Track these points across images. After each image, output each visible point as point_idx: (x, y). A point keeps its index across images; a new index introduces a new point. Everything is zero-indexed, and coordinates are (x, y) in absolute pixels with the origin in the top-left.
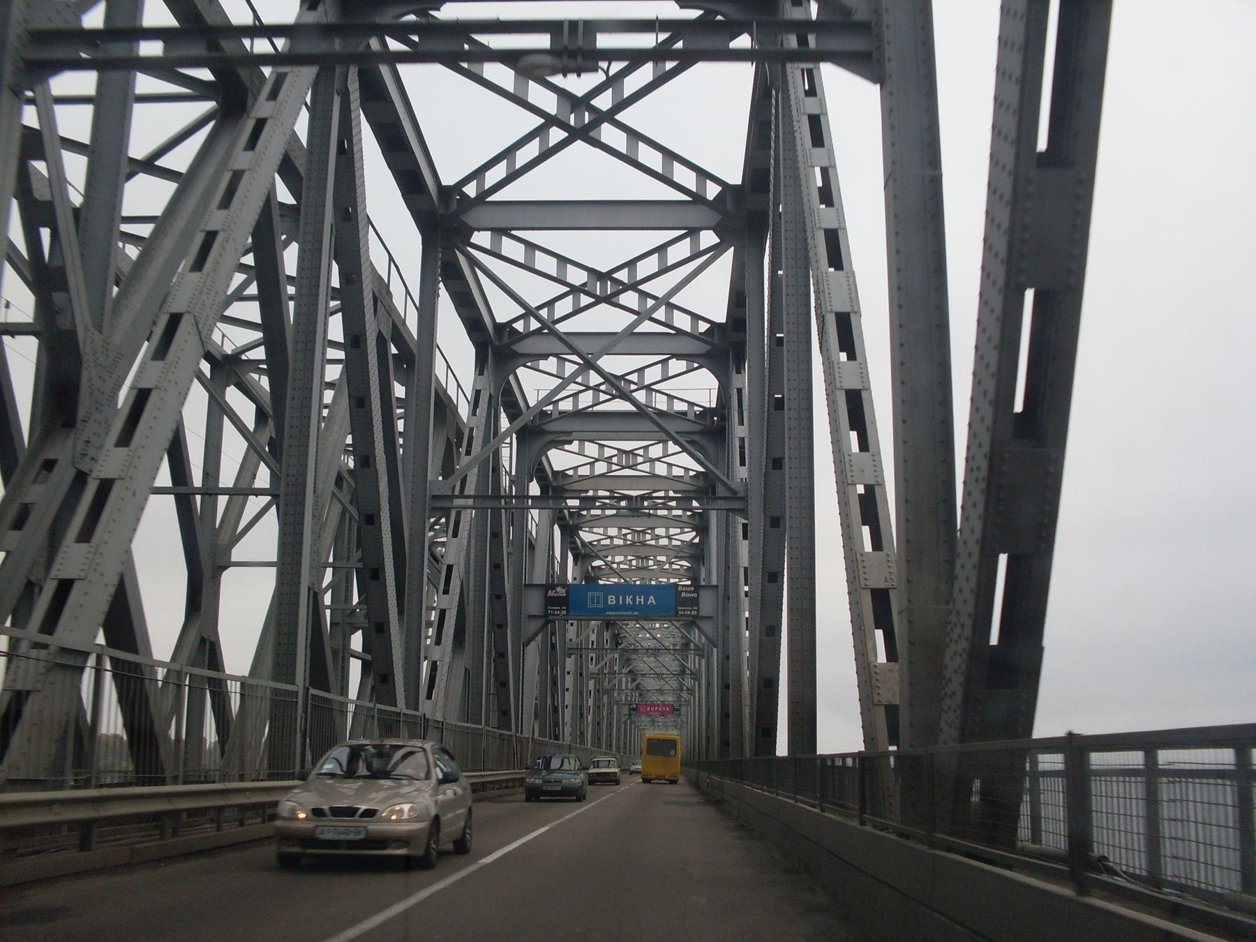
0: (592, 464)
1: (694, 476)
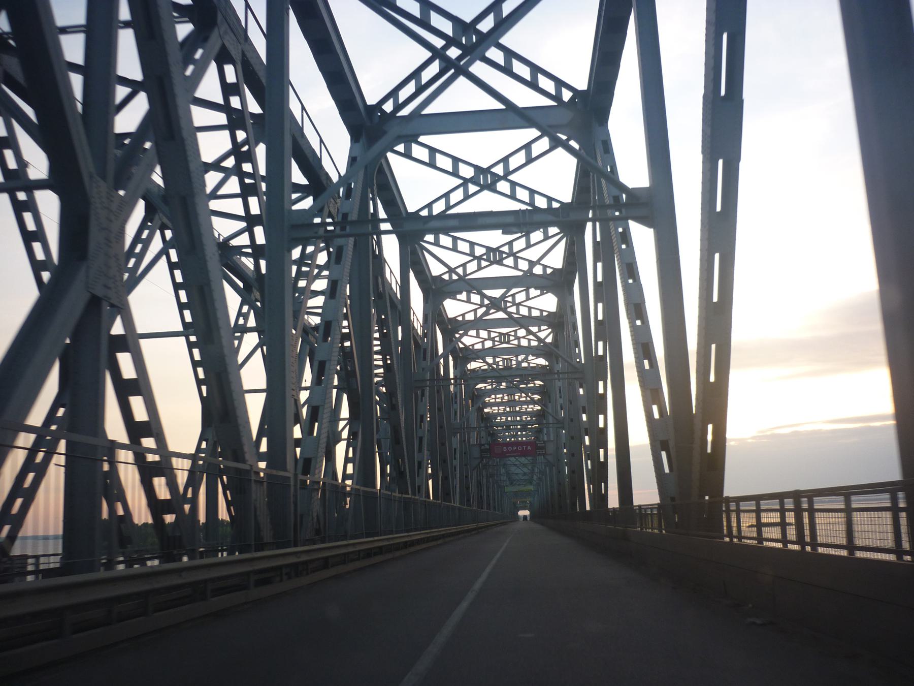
0: (483, 342)
1: (546, 315)
